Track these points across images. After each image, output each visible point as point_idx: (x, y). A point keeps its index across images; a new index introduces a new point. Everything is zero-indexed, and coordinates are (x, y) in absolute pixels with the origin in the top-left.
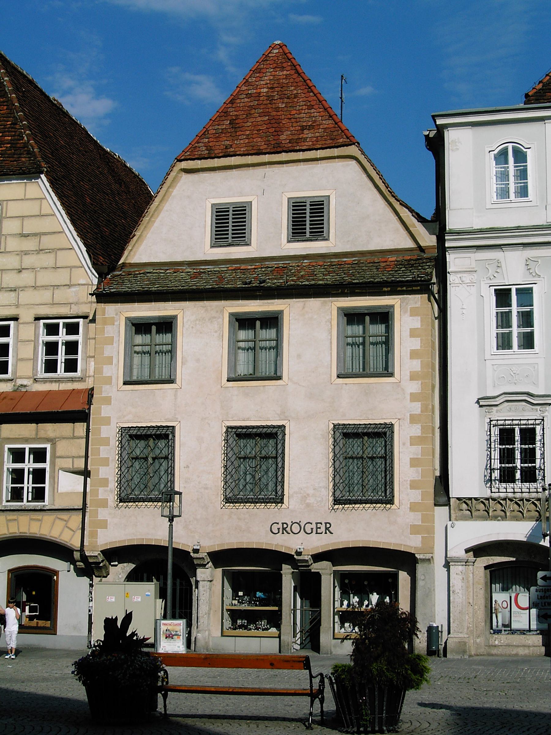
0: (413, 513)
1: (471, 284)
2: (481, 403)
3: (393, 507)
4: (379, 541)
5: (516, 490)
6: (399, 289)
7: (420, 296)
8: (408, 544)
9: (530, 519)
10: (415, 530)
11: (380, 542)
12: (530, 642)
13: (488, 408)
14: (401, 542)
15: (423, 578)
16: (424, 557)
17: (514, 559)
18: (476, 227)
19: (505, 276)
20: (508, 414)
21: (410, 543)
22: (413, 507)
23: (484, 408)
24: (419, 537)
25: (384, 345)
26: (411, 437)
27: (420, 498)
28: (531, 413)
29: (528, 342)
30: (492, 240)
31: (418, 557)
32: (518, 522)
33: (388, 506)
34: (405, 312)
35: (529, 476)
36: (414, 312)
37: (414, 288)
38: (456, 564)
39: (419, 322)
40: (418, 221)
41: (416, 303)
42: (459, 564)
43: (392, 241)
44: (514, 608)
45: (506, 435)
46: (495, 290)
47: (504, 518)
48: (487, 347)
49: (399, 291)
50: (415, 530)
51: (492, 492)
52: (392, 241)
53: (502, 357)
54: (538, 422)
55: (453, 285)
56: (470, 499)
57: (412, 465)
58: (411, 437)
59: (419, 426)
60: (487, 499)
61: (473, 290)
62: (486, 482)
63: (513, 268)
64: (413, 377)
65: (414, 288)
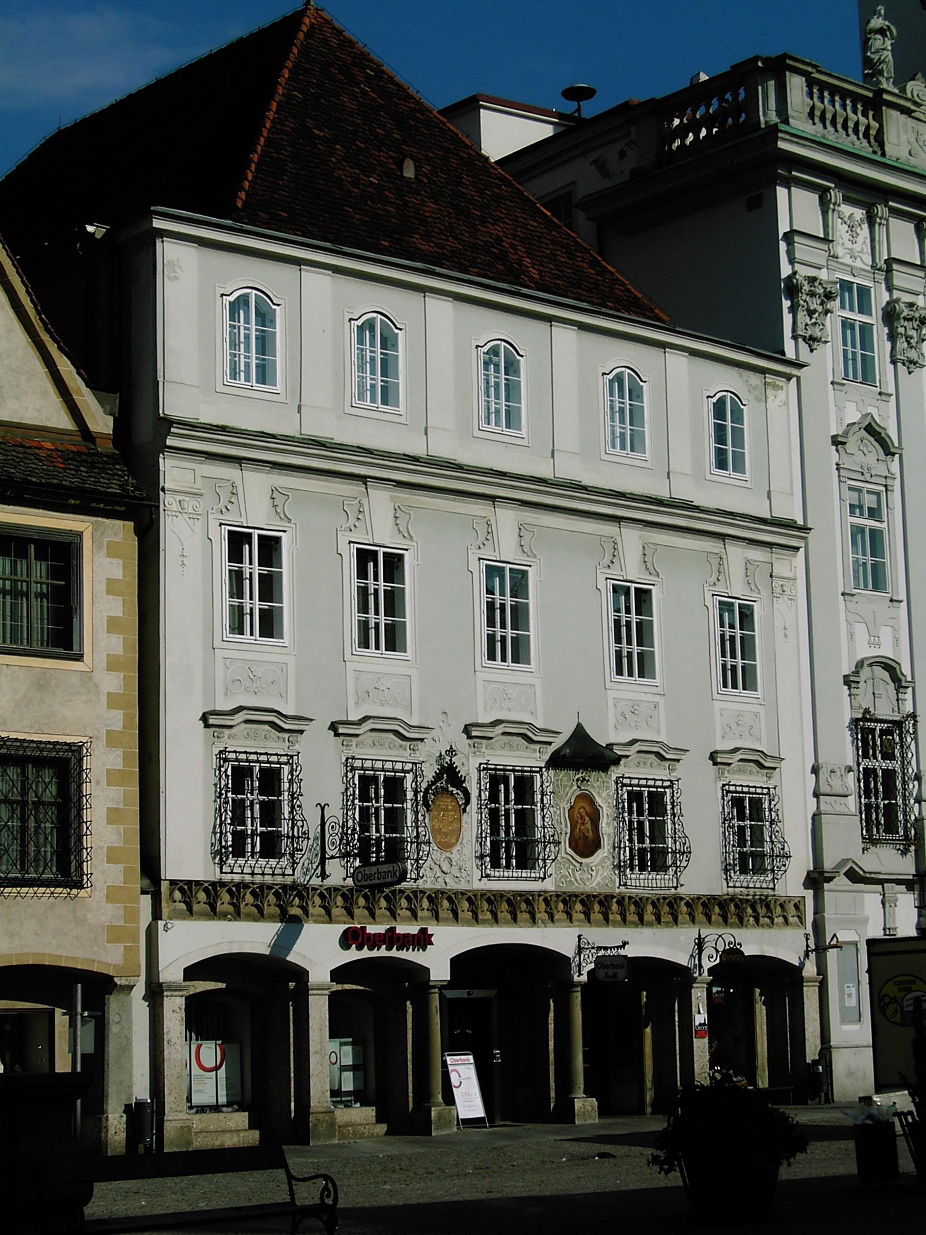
0: (111, 905)
1: (195, 516)
2: (211, 721)
3: (83, 893)
4: (59, 953)
5: (256, 871)
6: (94, 505)
7: (121, 523)
8: (104, 960)
9: (272, 918)
10: (115, 934)
11: (61, 956)
12: (232, 1125)
13: (217, 729)
14: (92, 957)
15: (117, 1019)
16: (127, 983)
17: (224, 986)
18: (204, 419)
19: (243, 511)
20: (245, 742)
21: (106, 958)
22: (112, 895)
23: (342, 738)
24: (121, 946)
25: (8, 597)
26: (108, 770)
27: (122, 879)
28: (275, 745)
29: (269, 625)
30: (231, 447)
31: (119, 983)
32: (256, 923)
33: (74, 891)
34: (100, 548)
35: (270, 848)
36: (113, 551)
37: (117, 508)
38: (174, 993)
39: (121, 567)
40: (87, 386)
41: (116, 534)
42: (177, 993)
43: (38, 410)
44: (196, 1069)
45: (241, 774)
46: (229, 531)
47: (237, 915)
48: (217, 629)
49: (93, 507)
50: (115, 934)
51: (222, 872)
52: (38, 410)
53: (237, 646)
54: (284, 759)
55: (170, 513)
56: (189, 883)
57: (111, 821)
58: (108, 770)
59: (120, 752)
60: (213, 884)
61: (198, 526)
62: (215, 854)
63: (255, 501)
64: (112, 665)
65: (117, 508)
